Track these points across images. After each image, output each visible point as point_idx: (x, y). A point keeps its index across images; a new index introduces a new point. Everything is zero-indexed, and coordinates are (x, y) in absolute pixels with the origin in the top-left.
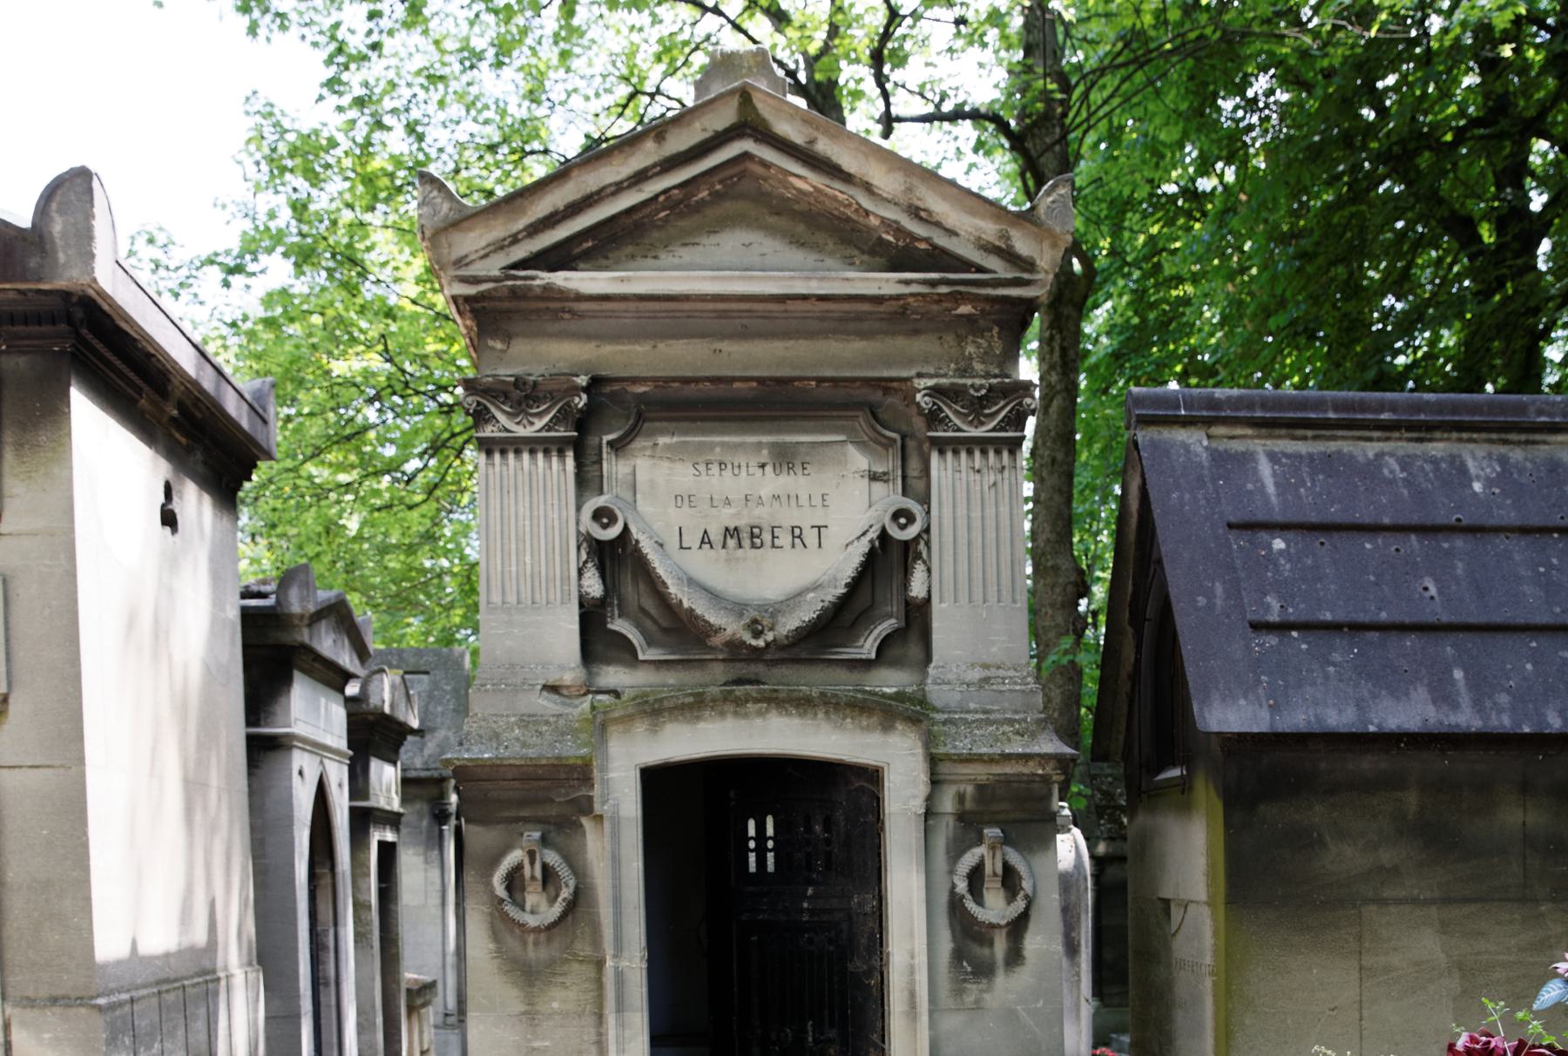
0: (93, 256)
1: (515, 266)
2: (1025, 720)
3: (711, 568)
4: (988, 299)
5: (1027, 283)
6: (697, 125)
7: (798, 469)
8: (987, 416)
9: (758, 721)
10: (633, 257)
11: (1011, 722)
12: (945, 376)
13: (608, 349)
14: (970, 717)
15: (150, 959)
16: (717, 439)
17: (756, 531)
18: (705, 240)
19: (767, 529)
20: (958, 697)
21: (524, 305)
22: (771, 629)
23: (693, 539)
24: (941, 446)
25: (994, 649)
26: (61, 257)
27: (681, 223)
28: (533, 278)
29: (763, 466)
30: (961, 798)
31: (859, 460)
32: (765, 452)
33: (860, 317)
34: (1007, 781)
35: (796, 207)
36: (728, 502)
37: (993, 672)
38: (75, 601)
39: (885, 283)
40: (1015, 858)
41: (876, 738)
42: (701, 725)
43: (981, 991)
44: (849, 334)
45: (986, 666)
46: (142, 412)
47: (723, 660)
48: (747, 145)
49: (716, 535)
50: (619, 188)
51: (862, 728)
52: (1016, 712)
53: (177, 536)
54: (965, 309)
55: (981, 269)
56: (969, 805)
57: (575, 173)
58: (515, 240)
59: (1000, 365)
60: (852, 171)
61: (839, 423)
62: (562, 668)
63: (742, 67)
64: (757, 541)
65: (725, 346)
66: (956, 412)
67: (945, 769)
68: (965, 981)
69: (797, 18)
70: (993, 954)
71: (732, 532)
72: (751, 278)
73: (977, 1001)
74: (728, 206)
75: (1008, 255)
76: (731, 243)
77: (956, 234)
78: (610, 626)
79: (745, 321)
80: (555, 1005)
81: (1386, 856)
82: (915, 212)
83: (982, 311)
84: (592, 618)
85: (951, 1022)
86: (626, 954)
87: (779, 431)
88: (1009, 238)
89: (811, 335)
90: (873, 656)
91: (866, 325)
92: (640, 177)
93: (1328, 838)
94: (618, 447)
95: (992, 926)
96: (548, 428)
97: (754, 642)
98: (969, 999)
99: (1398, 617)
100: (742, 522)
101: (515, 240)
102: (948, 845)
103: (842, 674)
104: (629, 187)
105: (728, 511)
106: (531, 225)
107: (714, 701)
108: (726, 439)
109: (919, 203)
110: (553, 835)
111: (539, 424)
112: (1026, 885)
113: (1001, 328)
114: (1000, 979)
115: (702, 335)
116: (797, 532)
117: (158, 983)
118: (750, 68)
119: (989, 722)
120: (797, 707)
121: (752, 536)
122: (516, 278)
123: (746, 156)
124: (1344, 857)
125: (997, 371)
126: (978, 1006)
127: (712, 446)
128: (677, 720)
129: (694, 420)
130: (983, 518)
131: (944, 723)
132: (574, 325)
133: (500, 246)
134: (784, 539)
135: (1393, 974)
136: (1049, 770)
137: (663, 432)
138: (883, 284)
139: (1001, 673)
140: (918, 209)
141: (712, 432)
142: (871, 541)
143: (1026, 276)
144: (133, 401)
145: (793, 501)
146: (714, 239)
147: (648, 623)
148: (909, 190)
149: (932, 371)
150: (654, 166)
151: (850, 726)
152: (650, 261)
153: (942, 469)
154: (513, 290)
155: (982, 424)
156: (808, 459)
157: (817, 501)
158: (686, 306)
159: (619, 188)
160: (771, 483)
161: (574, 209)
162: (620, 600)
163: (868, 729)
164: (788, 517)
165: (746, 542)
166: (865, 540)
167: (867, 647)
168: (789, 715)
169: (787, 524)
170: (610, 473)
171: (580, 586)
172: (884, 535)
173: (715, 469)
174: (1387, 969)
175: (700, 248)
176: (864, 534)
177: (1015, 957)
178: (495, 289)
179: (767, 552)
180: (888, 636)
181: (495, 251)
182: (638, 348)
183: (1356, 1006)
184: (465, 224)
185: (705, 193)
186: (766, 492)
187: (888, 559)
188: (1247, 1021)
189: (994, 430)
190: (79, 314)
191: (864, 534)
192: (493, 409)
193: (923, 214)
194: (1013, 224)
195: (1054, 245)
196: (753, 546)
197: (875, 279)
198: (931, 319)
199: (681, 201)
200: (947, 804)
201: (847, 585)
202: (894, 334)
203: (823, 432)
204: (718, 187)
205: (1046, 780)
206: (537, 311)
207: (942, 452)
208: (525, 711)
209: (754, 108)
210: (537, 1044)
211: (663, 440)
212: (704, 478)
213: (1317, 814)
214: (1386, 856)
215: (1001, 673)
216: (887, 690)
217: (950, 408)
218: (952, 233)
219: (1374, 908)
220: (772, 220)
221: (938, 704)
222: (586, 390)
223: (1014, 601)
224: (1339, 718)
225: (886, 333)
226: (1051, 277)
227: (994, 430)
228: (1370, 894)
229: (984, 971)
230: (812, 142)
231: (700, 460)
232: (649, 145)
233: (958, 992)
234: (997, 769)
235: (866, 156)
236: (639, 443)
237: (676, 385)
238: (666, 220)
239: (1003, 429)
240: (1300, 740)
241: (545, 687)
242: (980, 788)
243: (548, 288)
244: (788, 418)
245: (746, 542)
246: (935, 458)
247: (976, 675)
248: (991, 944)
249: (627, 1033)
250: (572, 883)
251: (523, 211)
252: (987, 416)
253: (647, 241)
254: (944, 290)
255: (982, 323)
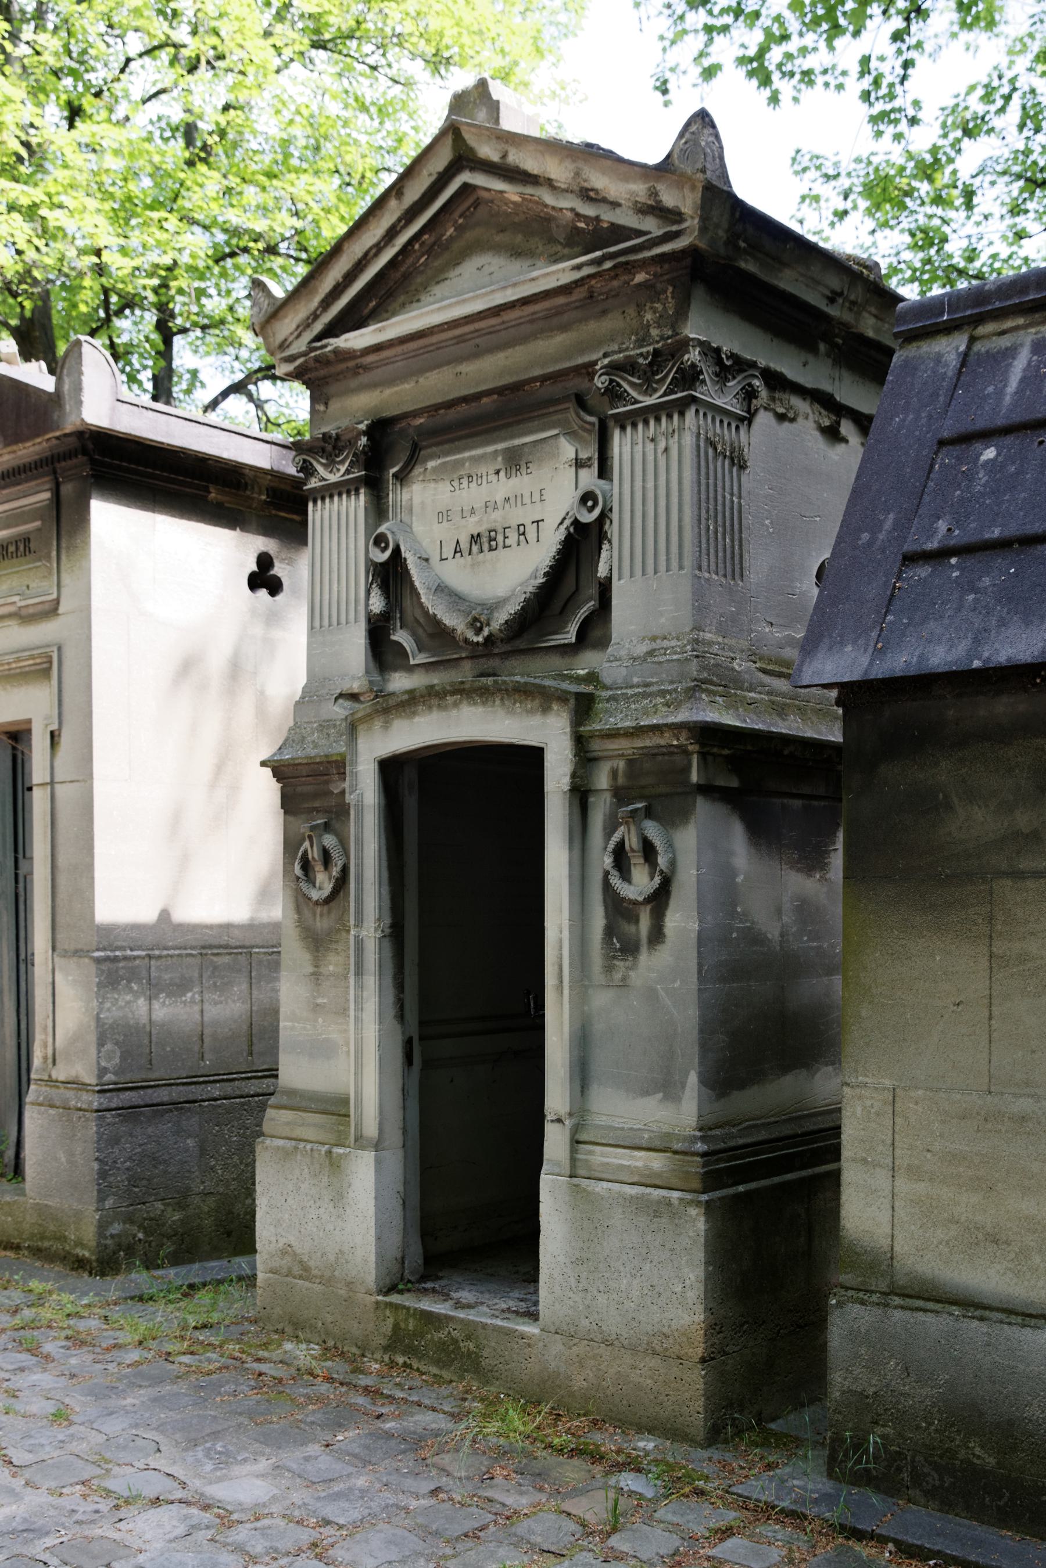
0: (81, 402)
1: (318, 338)
2: (675, 690)
3: (458, 574)
4: (662, 258)
5: (676, 235)
6: (425, 172)
7: (523, 470)
8: (658, 382)
9: (454, 712)
10: (403, 305)
11: (663, 693)
12: (627, 349)
13: (388, 392)
14: (630, 692)
15: (181, 928)
16: (467, 454)
17: (493, 534)
18: (452, 274)
19: (500, 530)
20: (624, 672)
21: (333, 369)
22: (488, 625)
23: (448, 552)
24: (624, 422)
25: (663, 620)
26: (68, 407)
27: (436, 264)
28: (325, 346)
29: (497, 472)
30: (614, 773)
31: (568, 450)
32: (500, 459)
33: (558, 312)
34: (651, 754)
35: (517, 219)
36: (473, 511)
37: (659, 644)
38: (90, 658)
39: (557, 274)
40: (652, 830)
41: (537, 720)
42: (417, 719)
43: (628, 968)
44: (552, 330)
45: (654, 639)
46: (219, 505)
47: (467, 658)
48: (465, 177)
49: (464, 545)
50: (379, 248)
51: (527, 711)
52: (672, 682)
53: (279, 598)
54: (640, 277)
55: (640, 233)
56: (621, 781)
57: (346, 246)
58: (315, 316)
59: (673, 327)
60: (535, 172)
61: (555, 418)
62: (353, 678)
63: (469, 102)
64: (493, 543)
65: (466, 368)
66: (632, 385)
67: (596, 746)
68: (614, 957)
69: (141, 107)
70: (638, 931)
71: (475, 539)
72: (464, 301)
73: (624, 978)
74: (470, 236)
75: (657, 210)
76: (469, 270)
77: (619, 205)
78: (393, 638)
79: (477, 341)
80: (331, 968)
81: (1024, 820)
82: (587, 194)
83: (655, 275)
84: (378, 633)
85: (601, 999)
86: (365, 924)
87: (513, 437)
88: (656, 194)
89: (524, 340)
90: (574, 640)
91: (565, 318)
92: (391, 234)
93: (956, 800)
94: (402, 478)
95: (635, 903)
96: (348, 472)
97: (475, 639)
98: (618, 976)
99: (1013, 529)
100: (482, 529)
101: (315, 316)
102: (605, 821)
103: (556, 662)
104: (386, 245)
105: (474, 519)
106: (323, 301)
107: (422, 696)
108: (473, 453)
109: (586, 185)
110: (334, 822)
111: (343, 469)
112: (662, 861)
113: (674, 287)
114: (644, 957)
115: (448, 363)
116: (522, 528)
117: (203, 947)
118: (475, 103)
119: (645, 695)
120: (481, 695)
121: (491, 540)
122: (316, 349)
123: (466, 188)
124: (973, 823)
125: (670, 333)
126: (624, 984)
127: (460, 463)
128: (401, 716)
129: (452, 441)
130: (644, 487)
131: (608, 701)
132: (364, 378)
133: (307, 324)
134: (512, 540)
135: (1029, 965)
136: (683, 740)
137: (432, 457)
138: (560, 275)
139: (666, 643)
140: (587, 190)
141: (460, 450)
142: (567, 528)
143: (675, 228)
144: (204, 499)
145: (519, 499)
146: (458, 270)
147: (420, 631)
148: (577, 174)
149: (616, 348)
150: (399, 220)
151: (519, 710)
152: (415, 305)
153: (621, 444)
154: (317, 359)
155: (655, 390)
156: (530, 458)
157: (536, 497)
158: (434, 339)
159: (379, 248)
160: (504, 486)
161: (350, 277)
162: (401, 613)
163: (531, 712)
164: (517, 515)
165: (486, 547)
166: (563, 527)
167: (570, 636)
168: (475, 704)
169: (514, 523)
170: (395, 502)
171: (367, 605)
172: (576, 523)
173: (465, 481)
174: (1023, 958)
175: (447, 282)
176: (561, 523)
177: (657, 935)
178: (306, 362)
179: (501, 552)
180: (586, 618)
181: (304, 330)
182: (407, 386)
183: (986, 1001)
184: (282, 313)
185: (452, 230)
186: (499, 498)
187: (582, 541)
188: (864, 1013)
189: (665, 395)
190: (90, 445)
191: (561, 523)
192: (315, 463)
193: (592, 194)
194: (658, 179)
195: (693, 188)
196: (491, 549)
197: (553, 273)
198: (617, 295)
199: (434, 244)
200: (602, 780)
201: (546, 574)
202: (585, 319)
203: (543, 430)
204: (461, 221)
205: (683, 751)
206: (342, 372)
207: (623, 428)
208: (325, 717)
209: (464, 140)
210: (319, 1001)
211: (431, 464)
212: (458, 492)
213: (942, 772)
214: (1024, 820)
215: (666, 643)
216: (581, 672)
217: (625, 379)
218: (615, 205)
219: (1009, 882)
220: (498, 238)
221: (607, 680)
222: (365, 433)
223: (681, 568)
224: (942, 655)
225: (580, 321)
226: (696, 221)
227: (665, 395)
228: (1004, 866)
229: (630, 949)
230: (504, 156)
231: (455, 476)
232: (393, 203)
233: (609, 969)
234: (639, 743)
235: (542, 153)
236: (418, 470)
237: (442, 411)
238: (425, 264)
239: (673, 392)
240: (922, 684)
241: (341, 696)
242: (630, 762)
243: (336, 352)
244: (519, 422)
245: (486, 547)
246: (617, 434)
247: (642, 649)
248: (637, 921)
249: (365, 994)
250: (340, 864)
251: (315, 291)
252: (658, 382)
253: (413, 288)
254: (608, 265)
255: (659, 286)
